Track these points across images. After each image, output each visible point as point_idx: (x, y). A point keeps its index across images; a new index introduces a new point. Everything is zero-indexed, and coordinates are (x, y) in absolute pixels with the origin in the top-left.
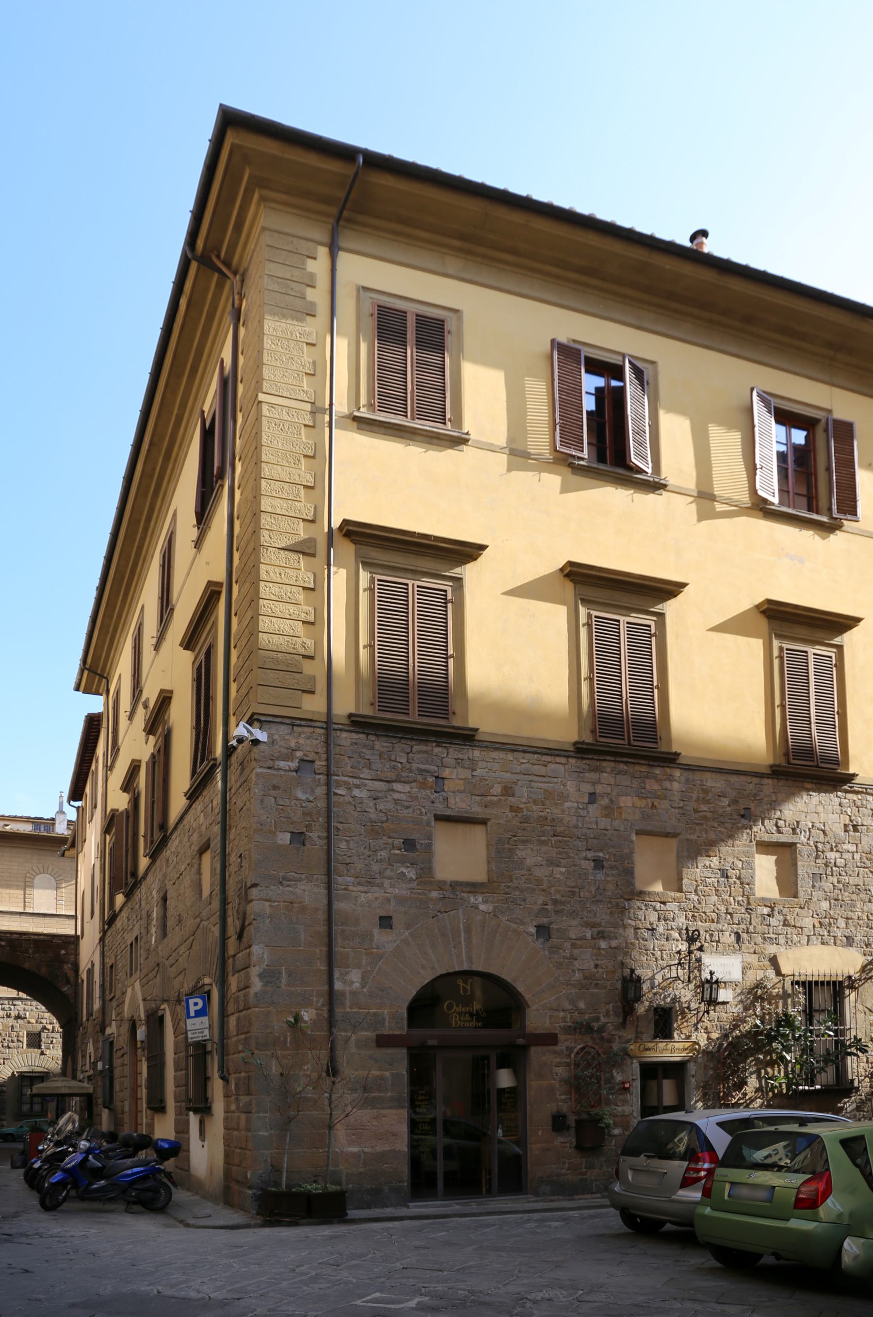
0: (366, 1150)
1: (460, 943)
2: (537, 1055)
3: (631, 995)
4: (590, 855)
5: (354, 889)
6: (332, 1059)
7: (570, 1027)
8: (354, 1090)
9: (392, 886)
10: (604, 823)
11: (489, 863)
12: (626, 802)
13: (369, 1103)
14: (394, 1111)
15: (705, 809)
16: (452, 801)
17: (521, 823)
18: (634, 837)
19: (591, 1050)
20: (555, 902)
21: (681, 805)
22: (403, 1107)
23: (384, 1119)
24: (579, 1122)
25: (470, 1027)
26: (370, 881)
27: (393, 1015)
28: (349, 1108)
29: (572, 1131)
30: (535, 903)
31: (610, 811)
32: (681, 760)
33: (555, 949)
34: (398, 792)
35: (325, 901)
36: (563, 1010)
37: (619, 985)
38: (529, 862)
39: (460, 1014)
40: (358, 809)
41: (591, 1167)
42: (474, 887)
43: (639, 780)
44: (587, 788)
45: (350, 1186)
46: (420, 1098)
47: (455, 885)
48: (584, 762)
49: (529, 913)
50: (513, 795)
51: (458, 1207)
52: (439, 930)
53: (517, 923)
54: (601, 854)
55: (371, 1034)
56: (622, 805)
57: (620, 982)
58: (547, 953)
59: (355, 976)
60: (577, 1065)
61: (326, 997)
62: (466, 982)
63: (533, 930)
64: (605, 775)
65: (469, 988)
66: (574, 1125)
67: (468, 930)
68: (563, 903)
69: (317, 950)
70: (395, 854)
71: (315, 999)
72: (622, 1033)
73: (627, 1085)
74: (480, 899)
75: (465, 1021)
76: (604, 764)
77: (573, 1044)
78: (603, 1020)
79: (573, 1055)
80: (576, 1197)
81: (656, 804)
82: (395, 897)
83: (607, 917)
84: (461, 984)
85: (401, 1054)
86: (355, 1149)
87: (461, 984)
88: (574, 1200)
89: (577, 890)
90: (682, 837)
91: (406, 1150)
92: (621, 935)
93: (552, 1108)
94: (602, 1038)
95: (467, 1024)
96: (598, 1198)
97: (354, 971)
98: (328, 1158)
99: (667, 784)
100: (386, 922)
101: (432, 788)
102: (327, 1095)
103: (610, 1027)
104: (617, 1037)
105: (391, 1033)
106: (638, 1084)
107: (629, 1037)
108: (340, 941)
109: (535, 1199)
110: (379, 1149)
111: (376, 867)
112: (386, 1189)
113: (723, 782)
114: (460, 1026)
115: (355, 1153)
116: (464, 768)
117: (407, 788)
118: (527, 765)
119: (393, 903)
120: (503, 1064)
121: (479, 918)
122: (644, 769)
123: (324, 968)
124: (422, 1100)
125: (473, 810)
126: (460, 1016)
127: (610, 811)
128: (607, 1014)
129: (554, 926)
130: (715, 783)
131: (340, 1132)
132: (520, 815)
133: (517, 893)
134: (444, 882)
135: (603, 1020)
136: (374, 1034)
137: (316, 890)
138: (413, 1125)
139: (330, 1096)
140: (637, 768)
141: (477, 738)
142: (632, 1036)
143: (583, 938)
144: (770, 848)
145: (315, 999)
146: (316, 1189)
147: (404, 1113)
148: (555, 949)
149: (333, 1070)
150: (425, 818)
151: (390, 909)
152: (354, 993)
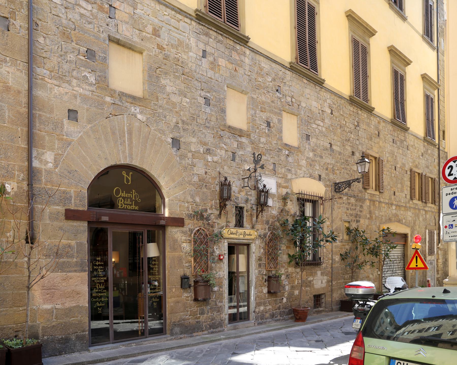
0: (57, 306)
1: (124, 141)
2: (173, 233)
3: (225, 195)
4: (203, 93)
5: (49, 81)
6: (31, 227)
7: (191, 214)
8: (48, 256)
9: (79, 86)
10: (210, 74)
11: (144, 84)
12: (222, 62)
13: (61, 267)
14: (78, 274)
15: (260, 80)
16: (120, 27)
17: (164, 59)
18: (226, 88)
19: (202, 232)
20: (183, 122)
21: (249, 74)
22: (85, 271)
23: (71, 280)
24: (196, 282)
25: (130, 210)
26: (62, 78)
27: (78, 194)
28: (44, 271)
29: (192, 288)
30: (171, 121)
31: (214, 65)
32: (249, 44)
33: (182, 157)
34: (83, 8)
35: (26, 86)
36: (188, 202)
37: (218, 188)
38: (168, 89)
39: (124, 198)
40: (53, 12)
41: (202, 313)
42: (134, 99)
43: (229, 50)
44: (202, 46)
45: (46, 337)
46: (97, 263)
47: (122, 95)
48: (200, 27)
49: (168, 127)
50: (159, 36)
51: (123, 347)
52: (111, 129)
53: (161, 133)
54: (208, 95)
55: (61, 209)
56: (220, 64)
57: (218, 186)
58: (178, 158)
59: (49, 156)
60: (195, 242)
61: (26, 173)
62: (128, 174)
63: (170, 140)
64: (211, 40)
65: (130, 179)
66: (193, 285)
67: (130, 133)
68: (187, 124)
69: (19, 129)
70: (80, 59)
71: (17, 173)
72: (219, 221)
73: (222, 258)
74: (138, 110)
75: (127, 205)
76: (211, 32)
77: (193, 227)
78: (209, 211)
79: (193, 235)
80: (194, 334)
81: (237, 69)
82: (80, 95)
83: (212, 140)
84: (125, 175)
85: (83, 226)
86: (48, 306)
87: (125, 175)
88: (193, 336)
89: (195, 116)
90: (249, 95)
91: (87, 305)
92: (219, 154)
93: (180, 272)
94: (208, 224)
95: (129, 207)
96: (206, 334)
97: (48, 152)
98: (27, 316)
99: (242, 57)
100: (72, 114)
101: (107, 13)
102: (26, 259)
103: (212, 217)
104: (216, 224)
105: (76, 208)
106: (226, 257)
107: (223, 225)
108: (38, 125)
109: (171, 337)
110: (67, 305)
111: (66, 67)
112: (73, 337)
113: (269, 66)
114: (124, 209)
115: (49, 310)
116: (129, 4)
117: (89, 7)
118: (168, 17)
119: (79, 100)
120: (151, 240)
121: (137, 124)
122: (231, 43)
123: (24, 145)
124: (99, 265)
125: (134, 39)
126: (124, 201)
127: (214, 65)
128: (211, 208)
129: (182, 140)
130: (266, 65)
131: (37, 293)
132: (163, 52)
133: (161, 111)
134: (115, 91)
135: (209, 211)
136: (64, 209)
137: (18, 73)
138: (92, 287)
139: (29, 259)
140: (228, 41)
141: (324, 85)
142: (224, 224)
143: (198, 152)
144: (122, 43)
145: (17, 173)
146: (17, 344)
147: (85, 276)
148: (182, 157)
149: (31, 239)
150: (102, 36)
151: (76, 104)
152: (49, 172)
